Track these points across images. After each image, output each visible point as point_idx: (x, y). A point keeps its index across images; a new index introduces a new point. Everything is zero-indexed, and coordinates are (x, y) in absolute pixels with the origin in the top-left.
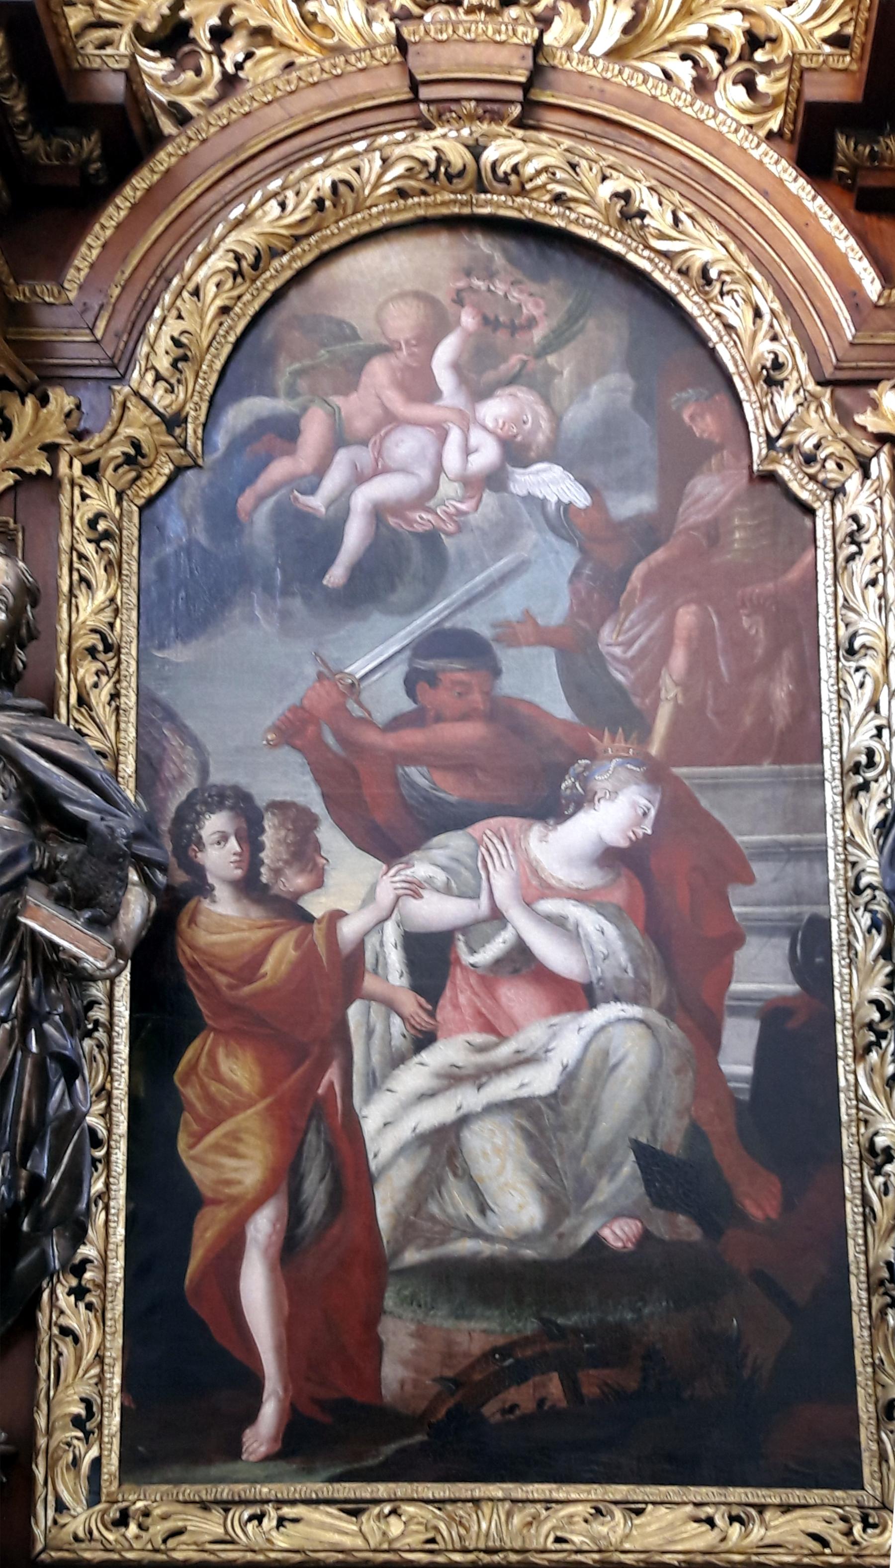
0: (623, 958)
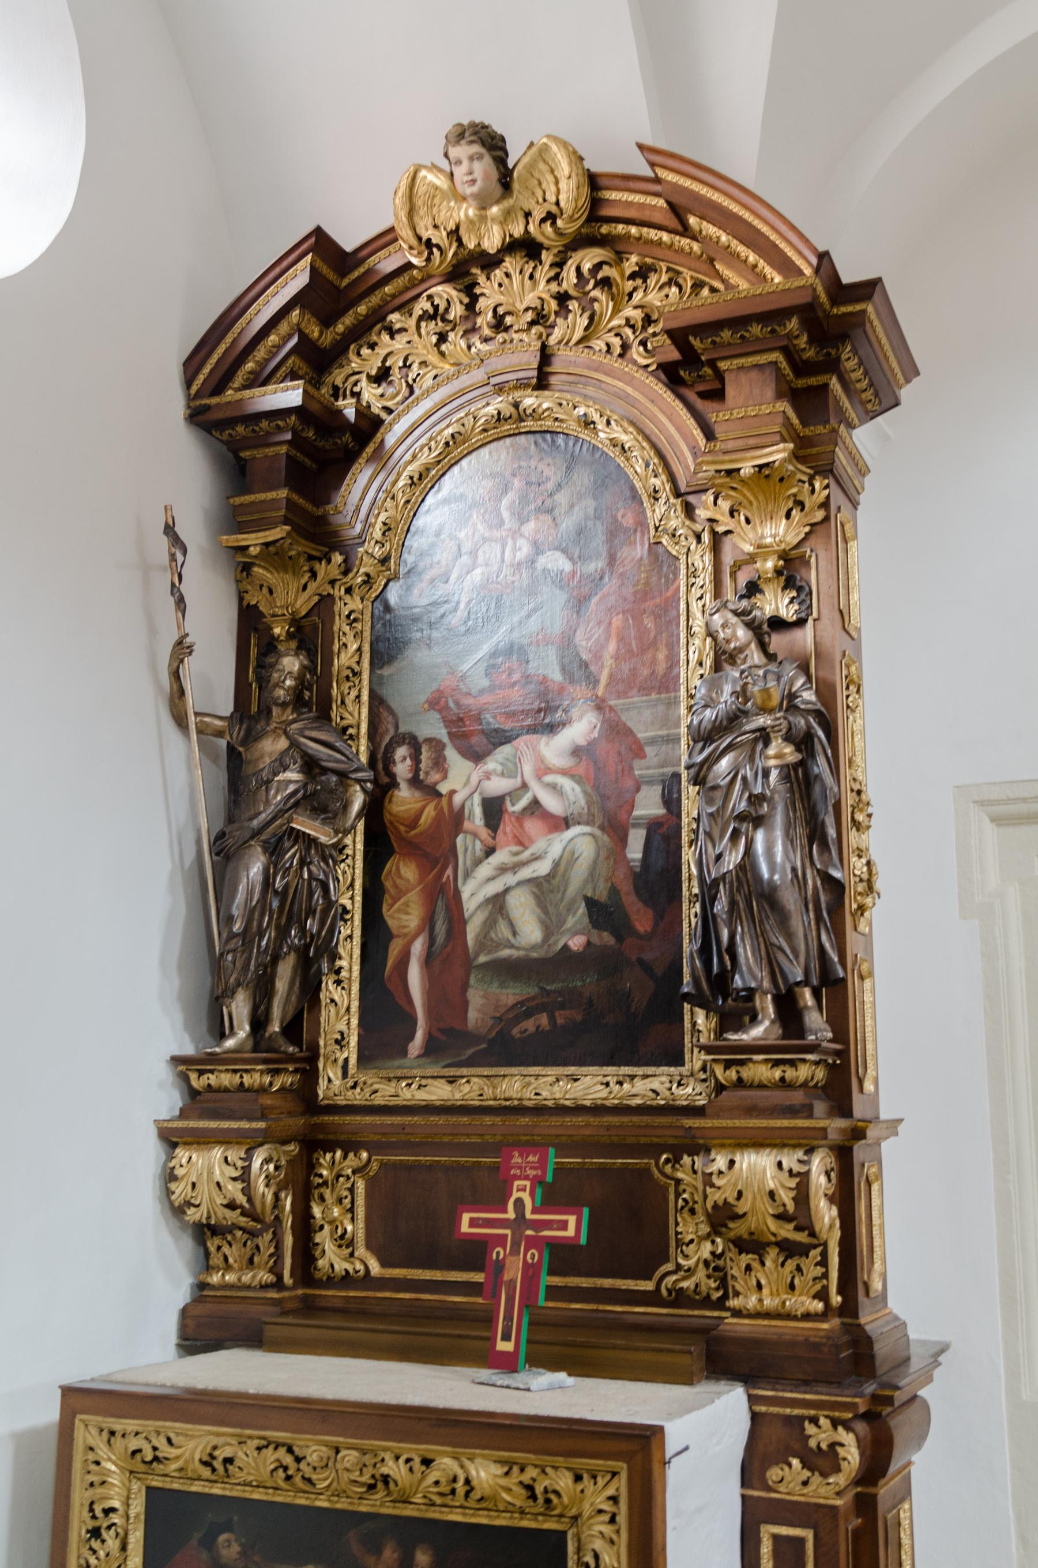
0: (583, 802)
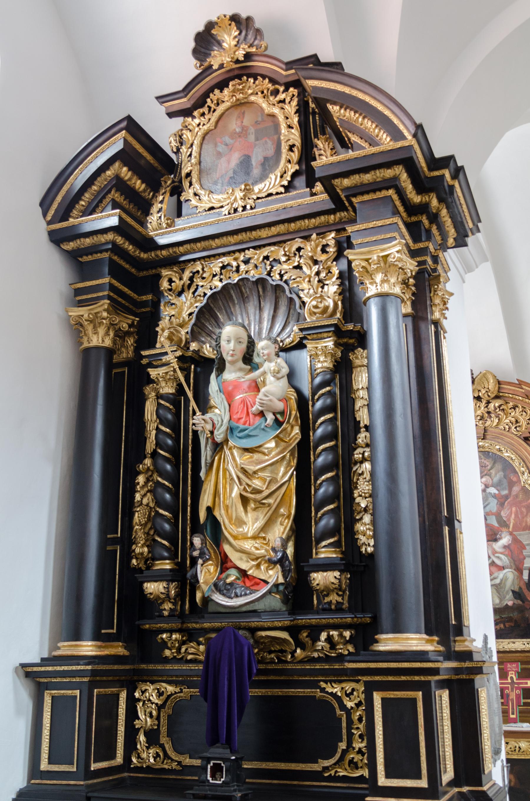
0: (508, 562)
